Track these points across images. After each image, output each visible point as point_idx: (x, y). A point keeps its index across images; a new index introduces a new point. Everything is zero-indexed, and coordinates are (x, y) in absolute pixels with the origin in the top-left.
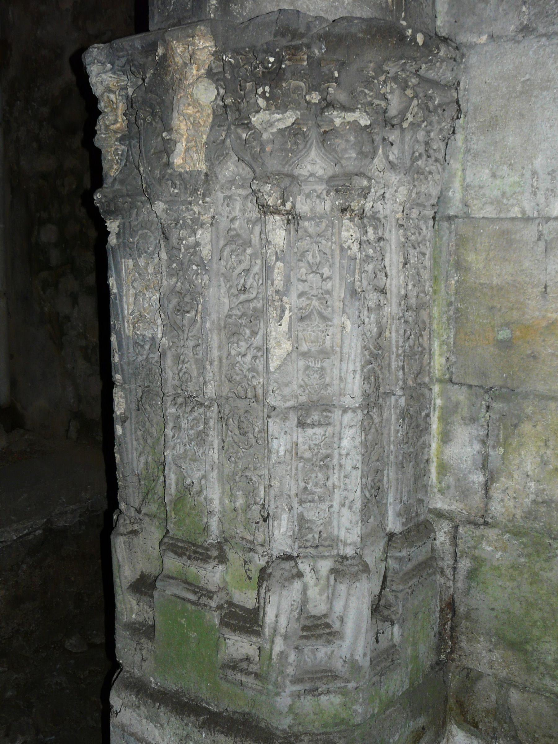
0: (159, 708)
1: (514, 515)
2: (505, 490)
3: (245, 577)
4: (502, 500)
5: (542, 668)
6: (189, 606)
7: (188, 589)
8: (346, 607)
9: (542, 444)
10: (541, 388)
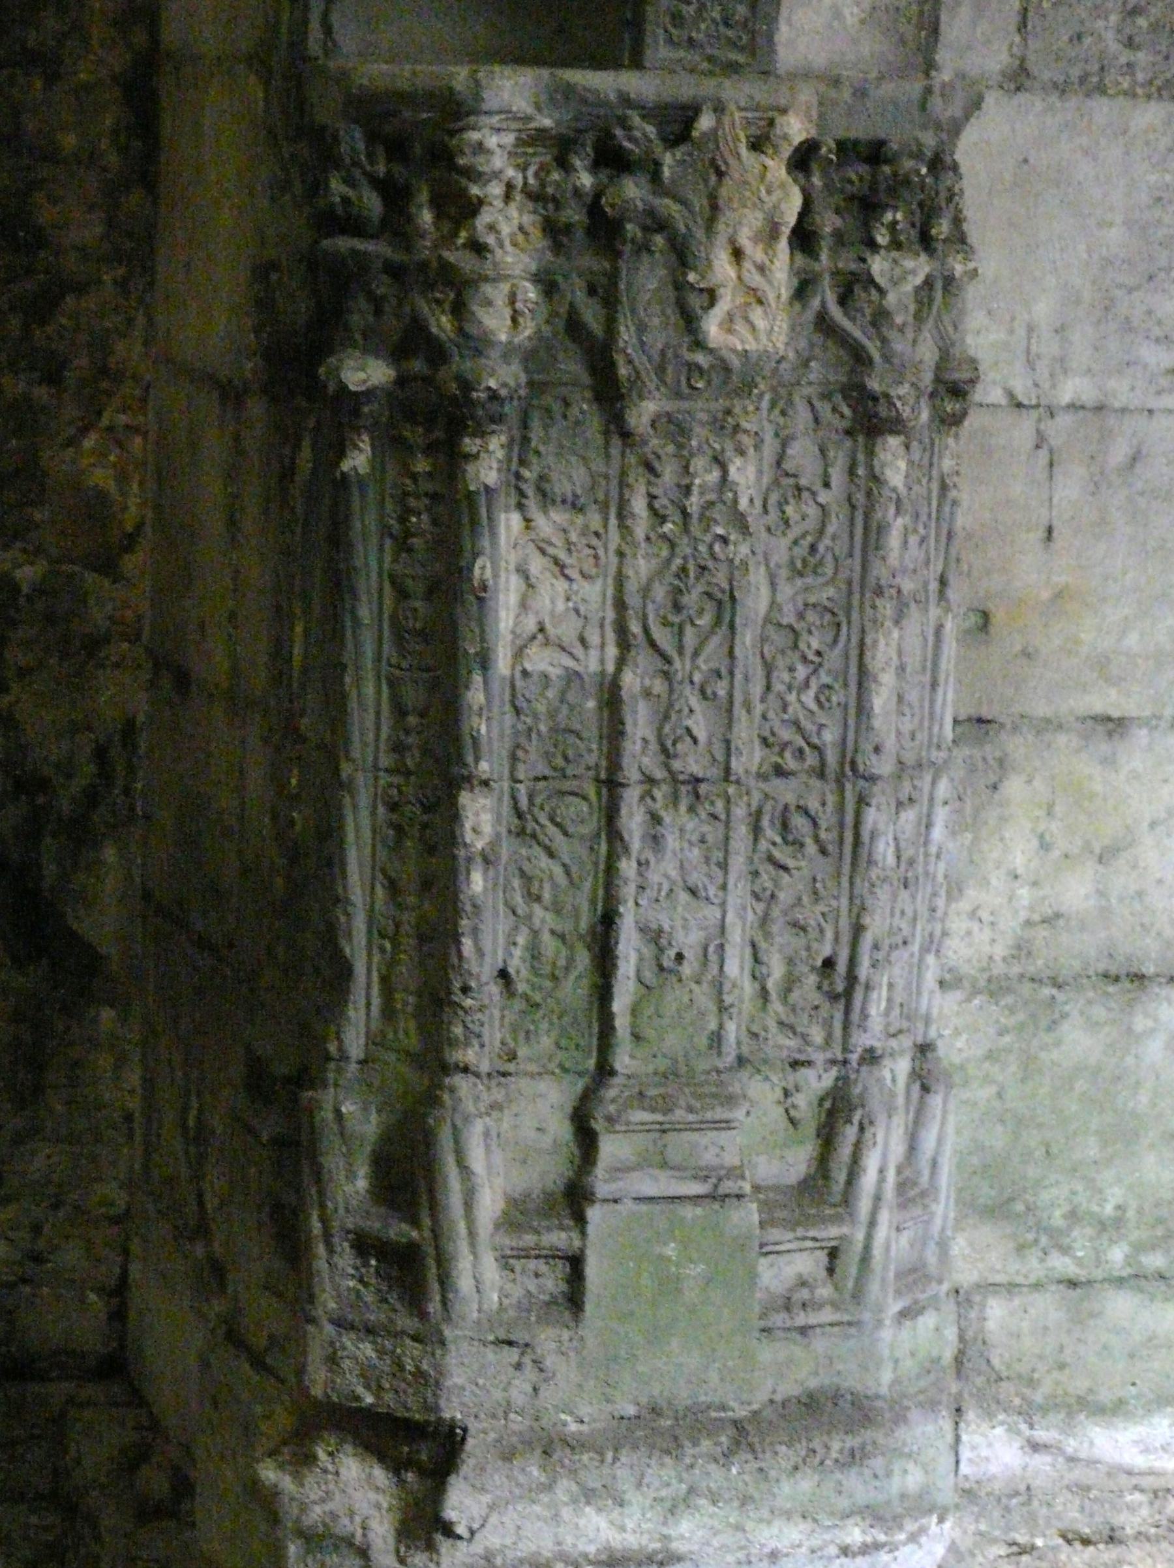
0: (616, 1459)
1: (991, 958)
2: (973, 914)
3: (784, 1123)
4: (969, 933)
5: (1044, 1240)
6: (689, 1212)
7: (681, 1178)
8: (940, 1141)
9: (1041, 813)
10: (1042, 709)
